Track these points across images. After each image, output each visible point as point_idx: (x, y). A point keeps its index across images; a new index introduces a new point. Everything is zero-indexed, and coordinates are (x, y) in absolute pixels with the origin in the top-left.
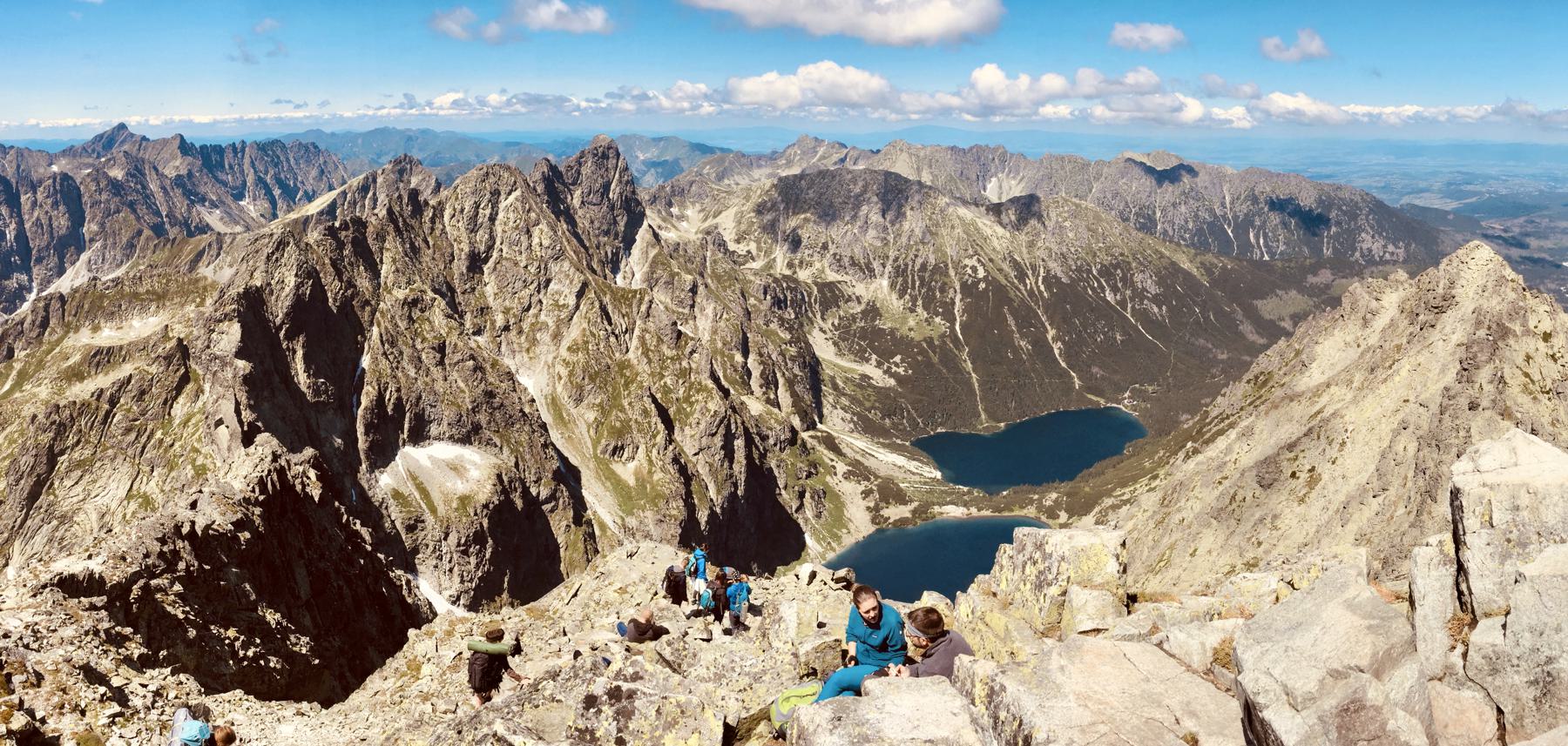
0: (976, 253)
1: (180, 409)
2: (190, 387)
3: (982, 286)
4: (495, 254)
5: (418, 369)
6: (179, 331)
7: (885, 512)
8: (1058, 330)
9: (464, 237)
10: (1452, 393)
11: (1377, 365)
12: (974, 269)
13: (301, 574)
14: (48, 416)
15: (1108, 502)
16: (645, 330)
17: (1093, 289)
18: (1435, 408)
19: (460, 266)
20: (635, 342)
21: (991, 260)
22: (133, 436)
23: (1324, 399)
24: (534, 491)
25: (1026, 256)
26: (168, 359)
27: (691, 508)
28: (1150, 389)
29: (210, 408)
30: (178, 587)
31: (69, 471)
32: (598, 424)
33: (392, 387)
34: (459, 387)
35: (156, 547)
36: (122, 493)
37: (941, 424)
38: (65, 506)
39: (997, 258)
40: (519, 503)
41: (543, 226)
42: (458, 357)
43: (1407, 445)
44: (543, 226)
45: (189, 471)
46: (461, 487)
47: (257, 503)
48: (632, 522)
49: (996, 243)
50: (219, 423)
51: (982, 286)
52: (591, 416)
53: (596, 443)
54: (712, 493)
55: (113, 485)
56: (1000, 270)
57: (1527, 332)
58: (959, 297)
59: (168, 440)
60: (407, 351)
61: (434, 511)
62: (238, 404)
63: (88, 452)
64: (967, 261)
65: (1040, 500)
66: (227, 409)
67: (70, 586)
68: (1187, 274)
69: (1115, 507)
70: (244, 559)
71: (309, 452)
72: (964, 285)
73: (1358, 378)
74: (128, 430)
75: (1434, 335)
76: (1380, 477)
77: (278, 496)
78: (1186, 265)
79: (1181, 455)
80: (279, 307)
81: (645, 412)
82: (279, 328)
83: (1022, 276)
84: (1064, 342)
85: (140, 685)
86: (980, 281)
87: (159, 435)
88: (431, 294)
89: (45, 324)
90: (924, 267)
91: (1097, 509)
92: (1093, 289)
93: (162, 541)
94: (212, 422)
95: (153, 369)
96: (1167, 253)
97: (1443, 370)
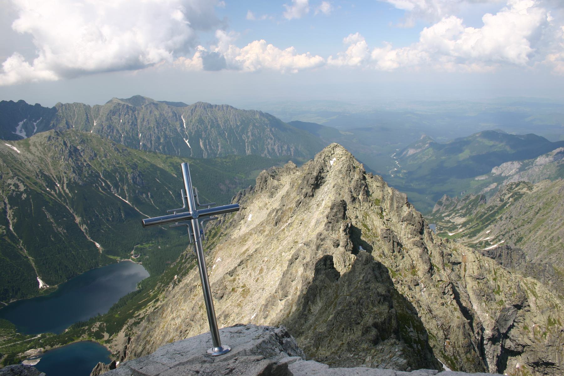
0: (15, 175)
3: (24, 196)
8: (82, 216)
10: (322, 237)
11: (278, 219)
12: (16, 186)
15: (131, 321)
17: (102, 187)
18: (314, 247)
21: (28, 178)
23: (249, 243)
25: (53, 171)
28: (147, 246)
37: (13, 297)
39: (33, 176)
49: (29, 166)
51: (24, 196)
56: (36, 183)
58: (8, 206)
64: (9, 181)
65: (89, 329)
68: (163, 171)
69: (136, 324)
72: (10, 198)
73: (268, 228)
78: (161, 165)
79: (171, 285)
83: (52, 185)
84: (87, 225)
86: (22, 193)
91: (125, 327)
92: (102, 187)
96: (148, 159)
97: (318, 222)
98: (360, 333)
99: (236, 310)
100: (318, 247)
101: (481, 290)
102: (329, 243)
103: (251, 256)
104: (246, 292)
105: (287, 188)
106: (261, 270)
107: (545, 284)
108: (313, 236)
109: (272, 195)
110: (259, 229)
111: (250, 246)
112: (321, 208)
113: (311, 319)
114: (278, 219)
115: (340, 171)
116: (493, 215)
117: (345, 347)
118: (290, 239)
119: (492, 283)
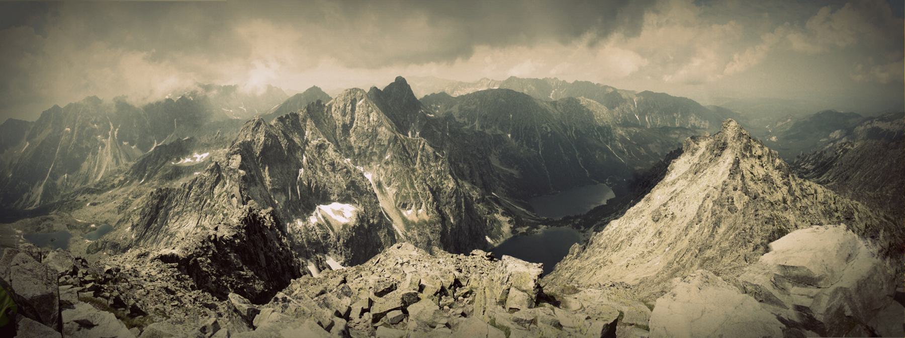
1: (217, 190)
2: (222, 182)
4: (354, 125)
5: (324, 173)
6: (216, 159)
7: (518, 229)
9: (340, 118)
11: (697, 170)
13: (262, 257)
14: (157, 193)
15: (599, 223)
16: (422, 156)
18: (720, 190)
19: (339, 131)
20: (418, 160)
22: (197, 202)
23: (677, 185)
24: (371, 221)
26: (212, 170)
27: (444, 226)
29: (229, 190)
30: (209, 261)
31: (173, 216)
32: (397, 195)
33: (313, 181)
34: (339, 179)
35: (200, 244)
36: (194, 225)
38: (172, 230)
40: (366, 226)
41: (374, 113)
42: (340, 167)
43: (709, 204)
44: (374, 113)
45: (221, 216)
46: (343, 221)
47: (243, 228)
48: (409, 234)
50: (233, 196)
52: (394, 191)
53: (396, 202)
54: (452, 221)
55: (191, 222)
57: (752, 156)
59: (212, 203)
60: (319, 166)
61: (333, 230)
62: (240, 188)
63: (180, 209)
66: (236, 190)
67: (164, 259)
70: (237, 249)
71: (270, 209)
73: (690, 176)
74: (196, 200)
75: (721, 159)
76: (699, 216)
77: (252, 223)
80: (258, 150)
81: (424, 189)
82: (258, 158)
83: (566, 130)
85: (188, 297)
87: (208, 201)
88: (327, 142)
89: (158, 157)
90: (525, 128)
93: (203, 243)
94: (230, 196)
95: (206, 175)
97: (723, 173)
98: (751, 249)
99: (667, 229)
100: (723, 190)
101: (826, 211)
102: (731, 188)
103: (678, 194)
104: (673, 217)
105: (703, 149)
106: (685, 204)
107: (863, 204)
108: (721, 182)
109: (693, 154)
110: (685, 176)
111: (678, 186)
112: (726, 164)
113: (717, 238)
114: (697, 170)
115: (734, 138)
116: (831, 163)
117: (742, 258)
118: (705, 184)
119: (833, 206)
